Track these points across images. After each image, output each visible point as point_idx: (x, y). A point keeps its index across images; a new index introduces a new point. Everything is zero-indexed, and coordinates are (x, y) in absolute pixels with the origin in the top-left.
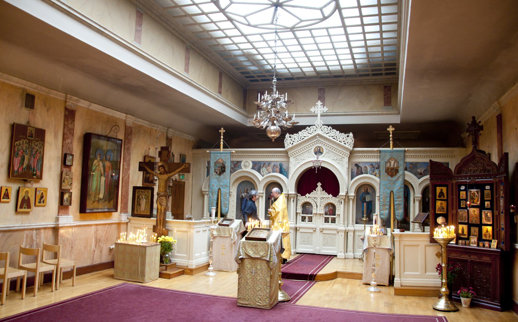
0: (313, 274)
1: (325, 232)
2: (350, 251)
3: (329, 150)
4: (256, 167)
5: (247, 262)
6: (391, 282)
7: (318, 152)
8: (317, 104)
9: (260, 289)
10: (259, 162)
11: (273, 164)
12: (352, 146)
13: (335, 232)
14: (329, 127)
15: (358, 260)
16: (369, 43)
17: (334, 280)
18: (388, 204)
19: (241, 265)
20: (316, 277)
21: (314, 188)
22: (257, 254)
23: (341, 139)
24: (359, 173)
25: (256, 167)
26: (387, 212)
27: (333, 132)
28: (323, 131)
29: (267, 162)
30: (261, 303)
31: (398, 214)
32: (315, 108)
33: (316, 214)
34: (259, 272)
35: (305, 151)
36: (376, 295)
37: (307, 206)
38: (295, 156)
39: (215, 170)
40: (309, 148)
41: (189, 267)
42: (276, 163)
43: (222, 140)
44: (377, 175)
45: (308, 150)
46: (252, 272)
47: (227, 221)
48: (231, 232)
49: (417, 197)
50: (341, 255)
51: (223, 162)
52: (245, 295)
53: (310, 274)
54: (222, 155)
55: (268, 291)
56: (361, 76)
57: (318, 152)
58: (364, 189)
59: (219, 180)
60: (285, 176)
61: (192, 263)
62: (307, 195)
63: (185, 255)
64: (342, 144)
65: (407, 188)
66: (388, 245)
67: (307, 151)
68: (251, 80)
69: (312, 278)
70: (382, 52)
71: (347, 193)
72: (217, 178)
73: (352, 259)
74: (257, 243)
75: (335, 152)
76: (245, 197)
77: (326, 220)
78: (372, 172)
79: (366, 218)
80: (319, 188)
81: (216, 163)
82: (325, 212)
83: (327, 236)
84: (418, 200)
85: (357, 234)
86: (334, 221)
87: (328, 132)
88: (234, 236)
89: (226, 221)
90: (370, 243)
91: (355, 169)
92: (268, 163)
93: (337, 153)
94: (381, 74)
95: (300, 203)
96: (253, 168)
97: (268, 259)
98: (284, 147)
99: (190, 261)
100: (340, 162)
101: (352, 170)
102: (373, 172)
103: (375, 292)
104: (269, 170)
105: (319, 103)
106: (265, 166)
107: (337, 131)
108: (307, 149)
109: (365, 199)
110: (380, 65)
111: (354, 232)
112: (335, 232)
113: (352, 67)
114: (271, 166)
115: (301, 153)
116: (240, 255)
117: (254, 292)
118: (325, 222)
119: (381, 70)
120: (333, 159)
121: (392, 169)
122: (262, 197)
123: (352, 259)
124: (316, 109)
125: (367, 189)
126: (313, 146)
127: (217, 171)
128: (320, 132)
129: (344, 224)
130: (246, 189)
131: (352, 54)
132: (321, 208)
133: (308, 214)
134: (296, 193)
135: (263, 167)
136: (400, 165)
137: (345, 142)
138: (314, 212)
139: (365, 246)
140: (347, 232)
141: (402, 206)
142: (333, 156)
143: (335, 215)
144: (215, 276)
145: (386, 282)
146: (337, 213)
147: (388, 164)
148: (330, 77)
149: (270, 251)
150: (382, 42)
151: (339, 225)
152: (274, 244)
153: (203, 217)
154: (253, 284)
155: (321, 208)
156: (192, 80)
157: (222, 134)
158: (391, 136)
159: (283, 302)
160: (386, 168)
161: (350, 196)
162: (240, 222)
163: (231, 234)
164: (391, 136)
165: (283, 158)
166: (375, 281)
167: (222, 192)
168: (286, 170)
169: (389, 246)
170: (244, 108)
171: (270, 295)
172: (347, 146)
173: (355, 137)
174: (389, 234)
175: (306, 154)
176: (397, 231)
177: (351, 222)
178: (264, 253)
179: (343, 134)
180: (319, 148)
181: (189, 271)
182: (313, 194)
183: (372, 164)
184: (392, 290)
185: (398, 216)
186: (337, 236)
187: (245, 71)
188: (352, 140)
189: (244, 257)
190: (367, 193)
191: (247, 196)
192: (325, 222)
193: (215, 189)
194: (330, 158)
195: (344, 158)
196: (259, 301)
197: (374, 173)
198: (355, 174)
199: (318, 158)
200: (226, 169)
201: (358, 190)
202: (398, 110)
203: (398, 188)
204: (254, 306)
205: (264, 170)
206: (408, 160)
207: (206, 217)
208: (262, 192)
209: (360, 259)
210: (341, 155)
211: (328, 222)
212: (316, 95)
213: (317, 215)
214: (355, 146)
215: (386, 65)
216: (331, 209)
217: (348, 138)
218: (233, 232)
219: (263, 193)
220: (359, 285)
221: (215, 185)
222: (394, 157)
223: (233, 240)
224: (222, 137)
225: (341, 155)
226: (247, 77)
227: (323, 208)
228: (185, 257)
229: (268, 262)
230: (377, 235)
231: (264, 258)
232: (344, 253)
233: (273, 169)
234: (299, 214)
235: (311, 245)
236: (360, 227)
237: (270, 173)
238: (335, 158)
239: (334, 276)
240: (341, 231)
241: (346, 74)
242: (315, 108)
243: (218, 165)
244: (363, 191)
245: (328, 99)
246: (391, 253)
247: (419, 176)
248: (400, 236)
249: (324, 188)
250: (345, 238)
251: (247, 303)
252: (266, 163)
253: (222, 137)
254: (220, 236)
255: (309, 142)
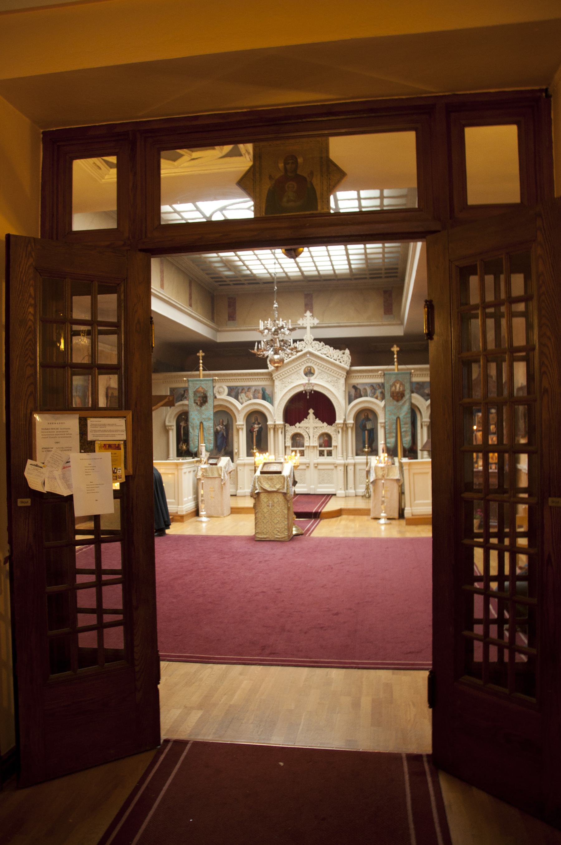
0: (317, 511)
1: (320, 467)
2: (351, 488)
3: (322, 371)
4: (233, 394)
5: (263, 497)
6: (401, 515)
7: (309, 372)
8: (305, 315)
9: (277, 521)
10: (237, 387)
11: (253, 389)
12: (349, 365)
13: (332, 467)
14: (320, 342)
15: (361, 498)
16: (368, 251)
17: (339, 518)
18: (395, 431)
19: (257, 499)
20: (320, 515)
21: (306, 415)
22: (273, 487)
23: (335, 357)
24: (357, 396)
25: (233, 394)
26: (393, 440)
27: (326, 349)
28: (314, 347)
29: (247, 386)
30: (279, 536)
31: (405, 442)
32: (303, 320)
33: (309, 447)
34: (275, 505)
35: (293, 372)
36: (387, 526)
37: (297, 438)
38: (281, 378)
39: (195, 400)
40: (298, 369)
41: (179, 513)
42: (257, 388)
43: (201, 365)
44: (379, 398)
45: (297, 371)
46: (268, 506)
47: (214, 460)
48: (220, 471)
49: (425, 422)
50: (341, 492)
51: (205, 390)
52: (263, 529)
53: (314, 511)
54: (203, 382)
55: (286, 523)
56: (356, 279)
57: (309, 372)
58: (365, 415)
59: (200, 412)
60: (270, 403)
61: (182, 508)
62: (297, 425)
63: (173, 501)
64: (337, 362)
65: (414, 411)
66: (396, 475)
67: (295, 372)
68: (220, 285)
69: (316, 516)
70: (384, 257)
71: (345, 420)
72: (197, 409)
73: (354, 497)
74: (272, 476)
75: (329, 372)
76: (220, 431)
77: (321, 453)
78: (373, 394)
79: (368, 448)
80: (311, 415)
81: (195, 393)
82: (319, 443)
83: (323, 471)
84: (426, 425)
85: (358, 467)
86: (330, 454)
87: (320, 349)
88: (224, 476)
89: (212, 460)
90: (378, 474)
91: (353, 392)
92: (248, 388)
93: (331, 373)
94: (381, 277)
95: (289, 435)
96: (229, 394)
97: (285, 491)
98: (267, 368)
99: (179, 507)
100: (336, 384)
101: (349, 393)
102: (374, 394)
103: (385, 524)
104: (249, 397)
105: (308, 314)
106: (244, 391)
107: (331, 347)
108: (295, 370)
109: (365, 426)
110: (381, 269)
111: (355, 465)
112: (332, 467)
113: (348, 271)
114: (251, 391)
115: (288, 374)
116: (256, 490)
117: (272, 525)
118: (320, 456)
119: (381, 274)
120: (328, 380)
121: (398, 393)
122: (242, 429)
123: (354, 497)
124: (304, 322)
125: (368, 415)
126: (302, 366)
127: (197, 401)
128: (311, 350)
129: (343, 457)
130: (221, 420)
131: (349, 260)
132: (315, 439)
133: (299, 447)
134: (284, 423)
135: (241, 393)
136: (406, 388)
137: (340, 361)
138: (306, 444)
139: (372, 478)
140: (347, 467)
141: (410, 433)
142: (326, 377)
143: (331, 446)
144: (209, 521)
145: (396, 515)
146: (334, 444)
147: (393, 388)
148: (320, 281)
149: (287, 483)
150: (384, 250)
151: (338, 458)
152: (290, 476)
153: (168, 457)
154: (270, 518)
155: (315, 439)
156: (170, 298)
157: (201, 358)
158: (395, 356)
159: (296, 535)
160: (391, 392)
161: (348, 424)
162: (227, 460)
163: (220, 473)
164: (395, 356)
165: (266, 381)
166: (385, 513)
167: (205, 427)
168: (270, 396)
169: (397, 476)
170: (212, 319)
171: (288, 527)
172: (342, 365)
173: (351, 354)
174: (397, 464)
175: (294, 376)
176: (405, 460)
177: (350, 454)
178: (280, 486)
179: (338, 350)
180: (309, 368)
181: (179, 518)
182: (304, 423)
183: (372, 386)
184: (403, 522)
185: (405, 443)
186: (334, 471)
187: (217, 276)
188: (348, 358)
189: (260, 491)
190: (367, 419)
191: (223, 429)
192: (320, 456)
193: (196, 423)
194: (323, 379)
195: (339, 379)
196: (278, 534)
197: (375, 396)
198: (353, 397)
199: (309, 381)
200: (208, 399)
201: (357, 417)
202: (402, 324)
203: (405, 413)
204: (273, 539)
205: (242, 396)
206: (415, 379)
207: (173, 457)
208: (241, 423)
209: (362, 496)
210: (336, 375)
211: (323, 455)
212: (301, 302)
213: (310, 448)
214: (352, 365)
215: (386, 269)
216: (326, 440)
217: (344, 355)
218: (223, 471)
219: (243, 425)
220: (368, 520)
221: (196, 418)
222: (400, 379)
223: (224, 480)
224: (201, 361)
225: (336, 375)
226: (212, 278)
227: (316, 439)
228: (172, 502)
229: (285, 494)
230: (385, 464)
231: (281, 491)
232: (345, 490)
233: (254, 395)
234: (288, 448)
235: (304, 483)
236: (362, 459)
237: (250, 399)
238: (329, 379)
239: (338, 513)
240: (340, 465)
241: (339, 277)
242: (303, 320)
243: (199, 395)
244: (362, 417)
245: (316, 308)
246: (400, 484)
247: (426, 397)
248: (410, 464)
249: (317, 415)
250: (344, 474)
251: (265, 536)
252: (245, 388)
253: (201, 361)
254: (208, 476)
255: (297, 361)
